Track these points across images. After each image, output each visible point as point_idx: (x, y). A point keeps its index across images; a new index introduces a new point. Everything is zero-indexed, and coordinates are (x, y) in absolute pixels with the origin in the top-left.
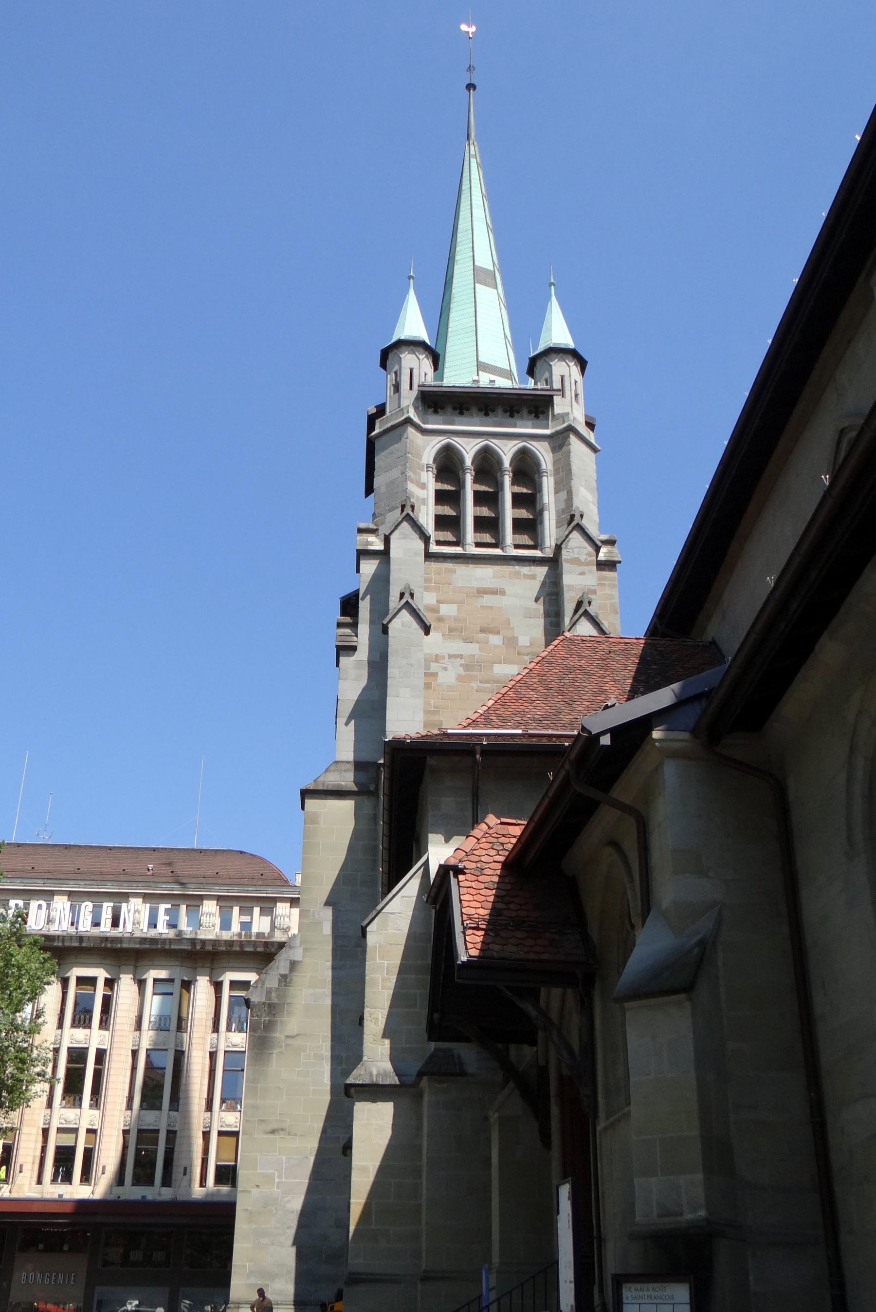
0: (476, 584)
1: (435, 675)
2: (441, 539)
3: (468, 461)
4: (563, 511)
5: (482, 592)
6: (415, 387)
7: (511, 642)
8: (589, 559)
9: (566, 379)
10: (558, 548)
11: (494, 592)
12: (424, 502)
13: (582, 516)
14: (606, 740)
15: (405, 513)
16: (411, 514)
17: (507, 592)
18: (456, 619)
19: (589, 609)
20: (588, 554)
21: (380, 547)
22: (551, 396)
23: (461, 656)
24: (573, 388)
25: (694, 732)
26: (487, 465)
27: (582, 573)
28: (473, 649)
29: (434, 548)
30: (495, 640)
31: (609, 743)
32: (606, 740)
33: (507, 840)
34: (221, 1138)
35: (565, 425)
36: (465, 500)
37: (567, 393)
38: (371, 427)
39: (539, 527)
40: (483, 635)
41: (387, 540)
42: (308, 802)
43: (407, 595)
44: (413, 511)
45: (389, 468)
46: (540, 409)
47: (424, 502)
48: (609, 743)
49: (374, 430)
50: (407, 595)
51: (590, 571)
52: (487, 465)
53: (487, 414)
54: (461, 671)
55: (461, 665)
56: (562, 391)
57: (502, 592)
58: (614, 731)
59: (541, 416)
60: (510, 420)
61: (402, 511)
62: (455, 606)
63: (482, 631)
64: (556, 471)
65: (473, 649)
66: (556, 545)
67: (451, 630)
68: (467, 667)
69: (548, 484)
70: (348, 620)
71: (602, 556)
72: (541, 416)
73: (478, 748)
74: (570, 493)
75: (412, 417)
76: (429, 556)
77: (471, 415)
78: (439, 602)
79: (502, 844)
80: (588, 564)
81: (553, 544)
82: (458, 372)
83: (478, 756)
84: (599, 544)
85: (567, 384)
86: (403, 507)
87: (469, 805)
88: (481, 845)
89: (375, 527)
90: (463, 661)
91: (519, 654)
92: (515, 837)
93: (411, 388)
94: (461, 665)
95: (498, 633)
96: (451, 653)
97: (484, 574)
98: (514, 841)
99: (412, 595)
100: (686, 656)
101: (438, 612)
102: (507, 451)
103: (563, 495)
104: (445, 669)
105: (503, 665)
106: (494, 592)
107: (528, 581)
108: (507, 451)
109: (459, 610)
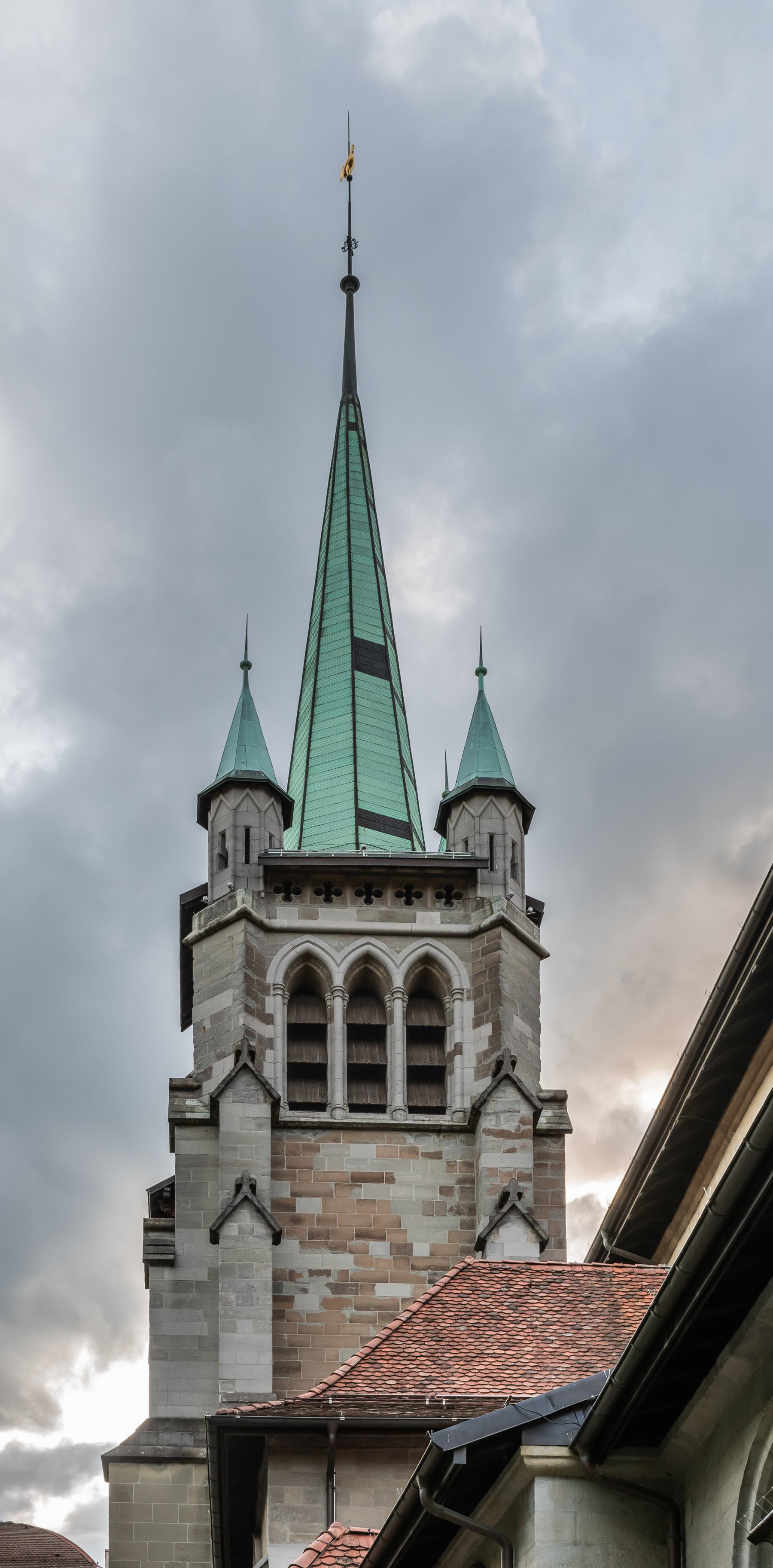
0: (350, 1169)
1: (290, 1299)
2: (298, 1100)
3: (338, 979)
4: (486, 1054)
5: (359, 1179)
6: (254, 858)
7: (402, 1251)
8: (523, 1128)
9: (498, 840)
10: (476, 1112)
11: (378, 1179)
12: (270, 1044)
13: (514, 1063)
14: (460, 1459)
15: (241, 1063)
16: (250, 1064)
17: (397, 1179)
18: (319, 1220)
19: (519, 1205)
20: (523, 1122)
21: (203, 1114)
22: (474, 870)
23: (328, 1273)
24: (509, 854)
25: (572, 1448)
26: (366, 984)
27: (512, 1151)
28: (344, 1262)
29: (286, 1114)
30: (379, 1249)
31: (465, 1462)
32: (460, 1459)
33: (354, 1553)
34: (278, 1134)
35: (492, 918)
36: (333, 1040)
37: (499, 865)
38: (186, 927)
39: (449, 1078)
40: (360, 1242)
41: (214, 1105)
42: (111, 1467)
43: (246, 1189)
44: (253, 1060)
45: (215, 992)
46: (454, 892)
47: (270, 1044)
48: (465, 1462)
49: (190, 930)
50: (246, 1189)
51: (523, 1147)
52: (366, 984)
53: (368, 901)
54: (328, 1293)
55: (328, 1285)
56: (489, 863)
57: (391, 1179)
58: (472, 1449)
59: (455, 901)
60: (407, 911)
61: (237, 1060)
62: (318, 1201)
63: (360, 1235)
64: (477, 993)
65: (344, 1262)
66: (473, 1108)
67: (312, 1236)
68: (336, 1288)
69: (462, 1011)
70: (162, 1222)
71: (543, 1122)
72: (455, 901)
73: (333, 1427)
74: (497, 1028)
75: (250, 909)
76: (277, 1125)
77: (344, 904)
78: (294, 1194)
79: (351, 1558)
80: (519, 1135)
81: (468, 1105)
82: (324, 828)
83: (332, 1436)
84: (538, 1104)
85: (498, 850)
86: (238, 1053)
87: (322, 1497)
88: (324, 1561)
89: (196, 1084)
90: (331, 1280)
91: (414, 1268)
92: (367, 1549)
93: (247, 861)
94: (328, 1285)
95: (383, 1238)
96: (314, 1267)
97: (363, 1153)
98: (364, 1554)
99: (253, 1188)
100: (641, 1289)
101: (293, 1208)
102: (398, 965)
103: (487, 1030)
104: (305, 1291)
105: (389, 1284)
106: (378, 1179)
107: (430, 1161)
108: (398, 965)
109: (325, 1206)
